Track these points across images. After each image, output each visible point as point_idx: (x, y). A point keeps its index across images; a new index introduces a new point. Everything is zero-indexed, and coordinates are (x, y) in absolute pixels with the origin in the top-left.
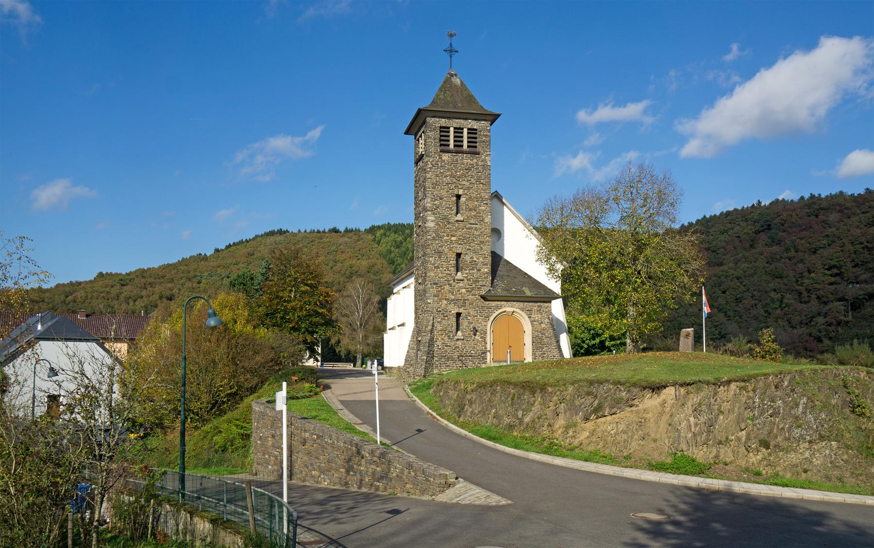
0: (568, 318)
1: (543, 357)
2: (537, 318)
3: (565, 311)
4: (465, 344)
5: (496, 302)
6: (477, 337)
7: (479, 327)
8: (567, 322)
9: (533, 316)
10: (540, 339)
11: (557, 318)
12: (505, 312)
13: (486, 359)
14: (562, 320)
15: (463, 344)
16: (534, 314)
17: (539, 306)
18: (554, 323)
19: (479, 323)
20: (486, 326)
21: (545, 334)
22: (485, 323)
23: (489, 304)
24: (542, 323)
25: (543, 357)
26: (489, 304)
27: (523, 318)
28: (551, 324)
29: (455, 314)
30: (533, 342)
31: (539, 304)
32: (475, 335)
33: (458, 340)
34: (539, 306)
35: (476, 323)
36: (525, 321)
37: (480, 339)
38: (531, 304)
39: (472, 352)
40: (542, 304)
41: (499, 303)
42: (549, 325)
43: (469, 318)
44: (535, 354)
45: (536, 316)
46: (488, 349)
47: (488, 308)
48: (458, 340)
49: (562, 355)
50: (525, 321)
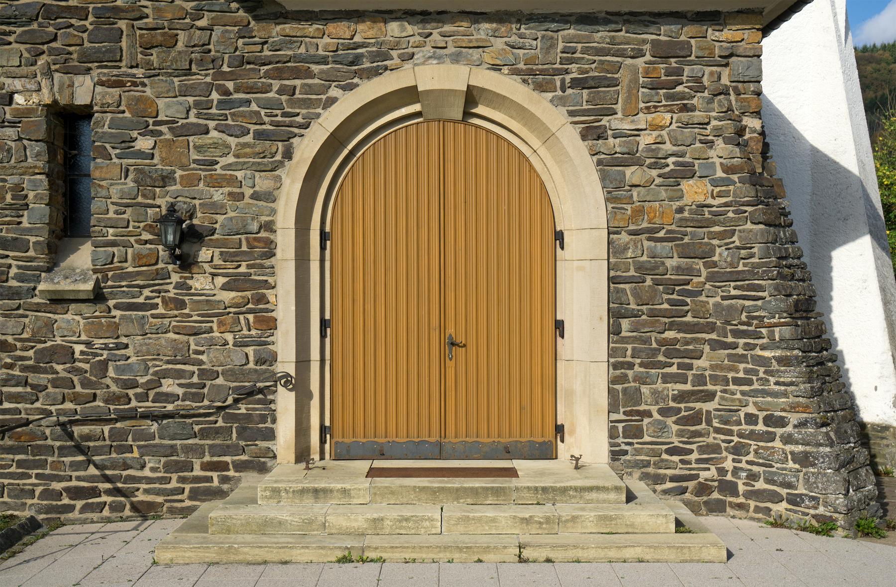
0: (885, 170)
1: (695, 418)
2: (646, 139)
3: (874, 150)
4: (114, 329)
5: (342, 29)
6: (199, 283)
7: (216, 208)
8: (881, 185)
9: (617, 123)
10: (670, 286)
11: (815, 151)
12: (410, 94)
13: (270, 435)
14: (853, 166)
15: (95, 329)
16: (631, 112)
17: (662, 53)
18: (781, 166)
19: (216, 182)
20: (269, 197)
21: (706, 255)
22: (263, 183)
23: (290, 40)
24: (686, 172)
25: (695, 418)
26: (290, 40)
27: (548, 137)
28: (754, 180)
29: (39, 119)
30: (616, 314)
31: (665, 33)
32: (186, 263)
33: (59, 301)
34: (662, 53)
35: (191, 181)
36: (561, 156)
37: (228, 296)
38: (601, 36)
39: (169, 386)
40: (686, 33)
41: (364, 31)
42: (740, 189)
43: (144, 144)
44: (634, 397)
45: (642, 120)
46: (286, 364)
47: (279, 74)
48: (59, 301)
49: (207, 236)
50: (561, 156)
